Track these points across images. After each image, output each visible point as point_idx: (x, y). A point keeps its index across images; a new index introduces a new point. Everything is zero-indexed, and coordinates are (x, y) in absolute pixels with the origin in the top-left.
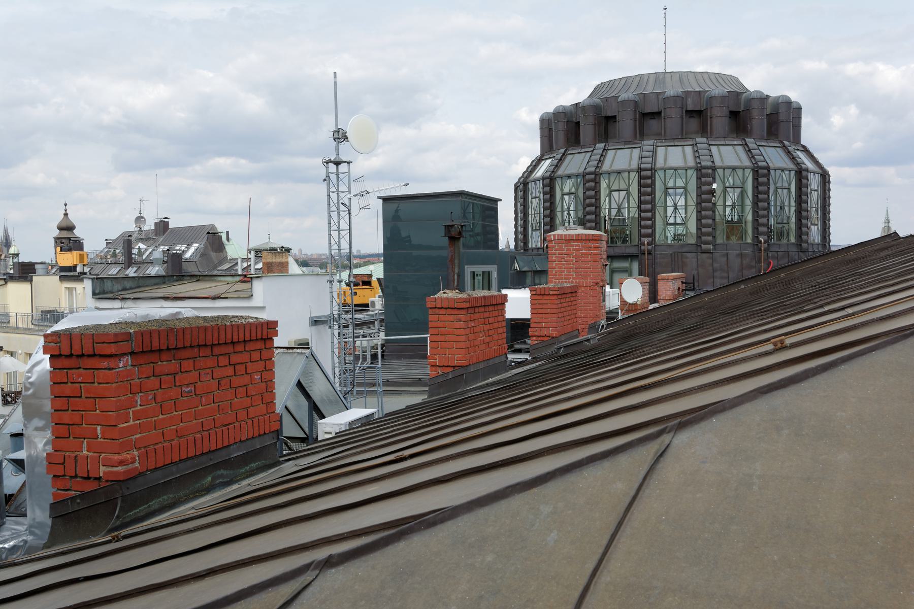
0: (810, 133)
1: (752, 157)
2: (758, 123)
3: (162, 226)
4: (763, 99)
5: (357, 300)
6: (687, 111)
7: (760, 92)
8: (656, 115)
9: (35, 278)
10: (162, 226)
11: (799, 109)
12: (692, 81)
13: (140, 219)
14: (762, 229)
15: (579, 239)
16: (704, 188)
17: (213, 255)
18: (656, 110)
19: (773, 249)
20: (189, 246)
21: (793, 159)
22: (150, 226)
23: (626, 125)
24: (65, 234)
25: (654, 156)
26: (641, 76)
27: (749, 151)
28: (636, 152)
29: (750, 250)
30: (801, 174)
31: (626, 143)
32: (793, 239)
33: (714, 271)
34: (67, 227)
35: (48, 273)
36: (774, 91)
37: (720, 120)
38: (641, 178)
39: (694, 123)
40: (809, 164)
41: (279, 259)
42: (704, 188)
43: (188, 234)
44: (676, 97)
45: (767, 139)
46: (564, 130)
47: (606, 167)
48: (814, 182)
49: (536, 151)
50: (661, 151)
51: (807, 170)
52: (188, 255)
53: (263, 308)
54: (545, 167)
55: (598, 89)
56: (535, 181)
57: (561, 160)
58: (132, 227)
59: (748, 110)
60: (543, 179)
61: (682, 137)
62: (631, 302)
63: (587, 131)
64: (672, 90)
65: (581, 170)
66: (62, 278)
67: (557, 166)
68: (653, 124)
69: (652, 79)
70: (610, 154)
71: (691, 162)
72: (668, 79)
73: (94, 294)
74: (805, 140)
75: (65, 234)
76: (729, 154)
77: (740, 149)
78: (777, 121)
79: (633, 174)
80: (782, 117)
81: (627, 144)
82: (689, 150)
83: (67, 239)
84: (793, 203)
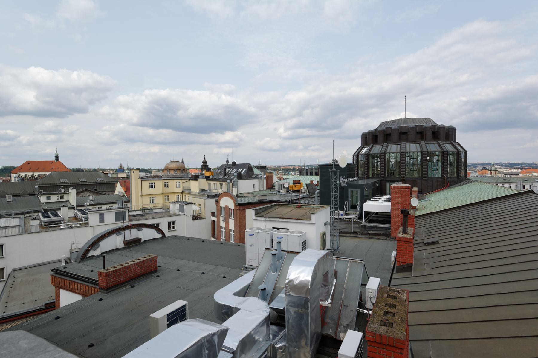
0: (460, 138)
1: (441, 148)
2: (443, 135)
3: (234, 163)
4: (443, 127)
5: (296, 189)
6: (417, 132)
7: (431, 120)
8: (406, 133)
9: (199, 180)
10: (234, 163)
11: (456, 130)
12: (418, 122)
13: (227, 161)
14: (445, 172)
15: (403, 188)
16: (424, 158)
17: (250, 173)
18: (405, 131)
19: (449, 179)
20: (243, 170)
21: (456, 148)
22: (230, 163)
23: (395, 136)
24: (205, 165)
25: (406, 148)
26: (399, 119)
27: (440, 146)
28: (399, 146)
29: (440, 180)
30: (459, 153)
31: (395, 143)
32: (455, 175)
33: (427, 186)
34: (205, 162)
35: (203, 178)
36: (447, 124)
37: (429, 135)
38: (401, 155)
39: (419, 136)
40: (461, 149)
41: (271, 175)
42: (424, 158)
43: (242, 166)
44: (413, 128)
45: (446, 141)
46: (370, 138)
47: (388, 151)
48: (463, 155)
49: (359, 145)
50: (408, 146)
51: (461, 151)
52: (242, 173)
53: (314, 224)
54: (365, 150)
55: (382, 124)
56: (362, 155)
57: (371, 148)
58: (225, 163)
59: (438, 131)
60: (365, 154)
61: (413, 141)
62: (414, 206)
63: (380, 139)
64: (411, 125)
65: (379, 152)
66: (207, 180)
67: (370, 150)
68: (404, 136)
69: (403, 121)
70: (389, 147)
71: (419, 150)
72: (409, 121)
73: (255, 215)
74: (457, 140)
75: (205, 165)
76: (433, 147)
77: (436, 145)
78: (447, 134)
79: (398, 154)
80: (450, 133)
81: (395, 143)
82: (418, 145)
83: (205, 166)
84: (455, 163)
